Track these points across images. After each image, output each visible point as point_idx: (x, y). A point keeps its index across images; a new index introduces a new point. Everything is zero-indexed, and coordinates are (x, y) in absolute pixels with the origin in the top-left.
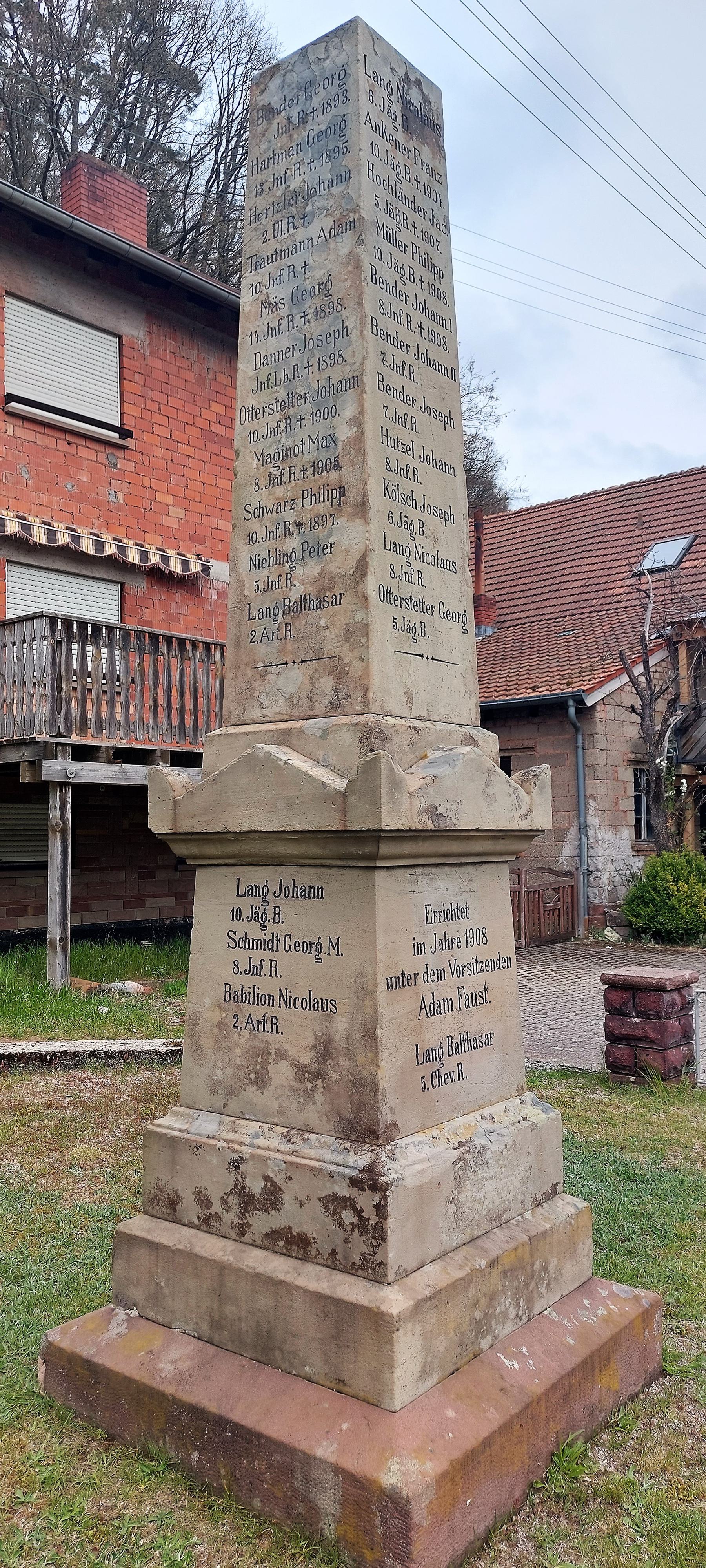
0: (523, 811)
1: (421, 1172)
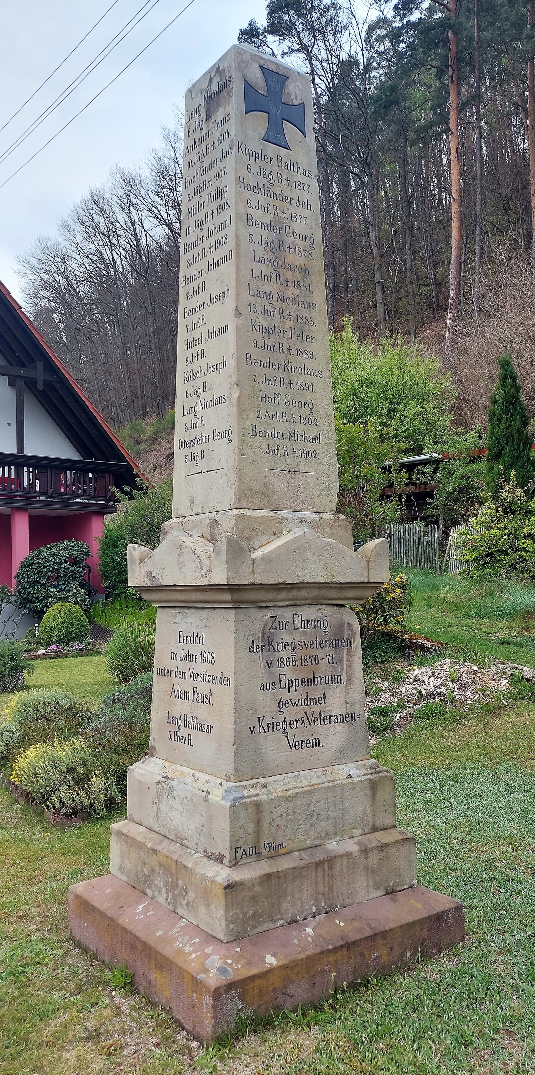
0: (204, 571)
1: (141, 774)
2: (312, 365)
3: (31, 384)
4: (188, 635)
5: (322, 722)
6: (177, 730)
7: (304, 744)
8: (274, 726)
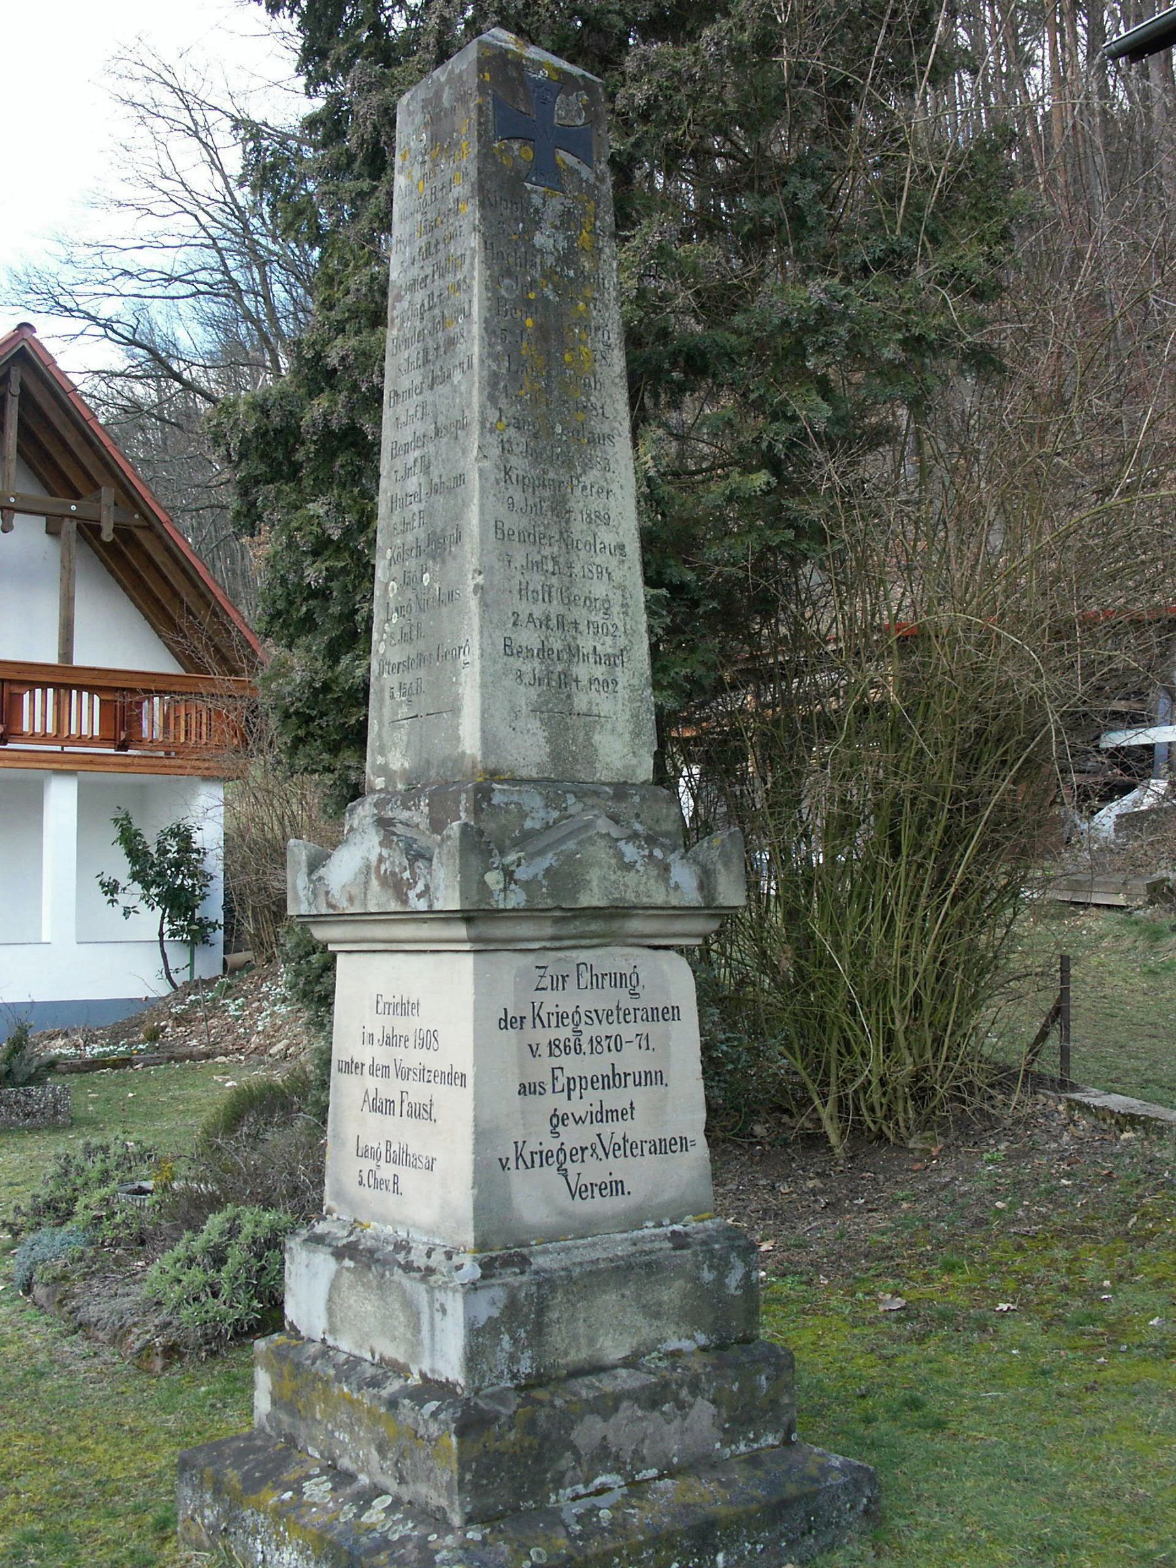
2: (607, 537)
3: (89, 531)
4: (391, 1000)
5: (628, 1152)
6: (374, 1168)
7: (596, 1190)
8: (545, 1157)
